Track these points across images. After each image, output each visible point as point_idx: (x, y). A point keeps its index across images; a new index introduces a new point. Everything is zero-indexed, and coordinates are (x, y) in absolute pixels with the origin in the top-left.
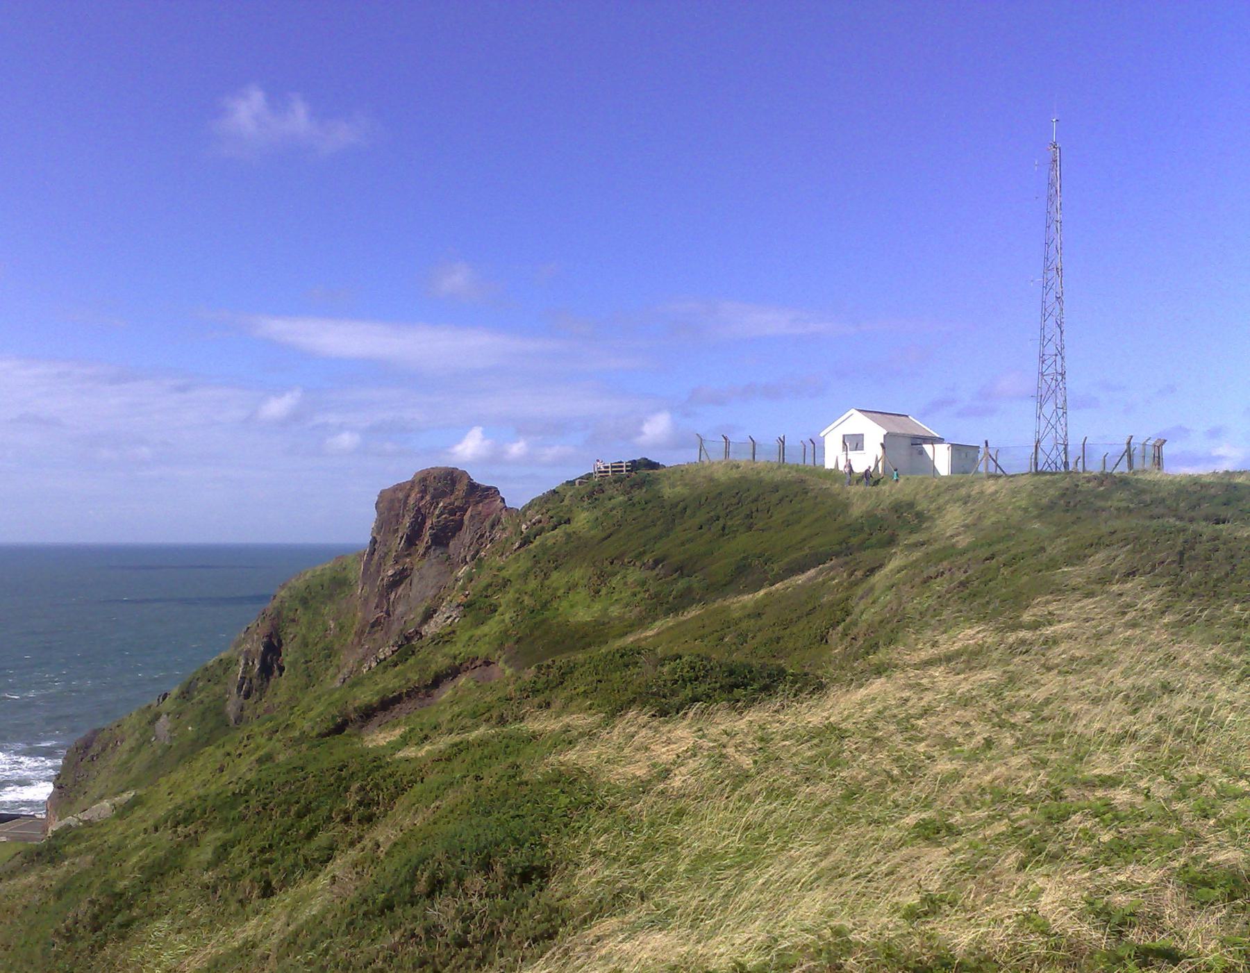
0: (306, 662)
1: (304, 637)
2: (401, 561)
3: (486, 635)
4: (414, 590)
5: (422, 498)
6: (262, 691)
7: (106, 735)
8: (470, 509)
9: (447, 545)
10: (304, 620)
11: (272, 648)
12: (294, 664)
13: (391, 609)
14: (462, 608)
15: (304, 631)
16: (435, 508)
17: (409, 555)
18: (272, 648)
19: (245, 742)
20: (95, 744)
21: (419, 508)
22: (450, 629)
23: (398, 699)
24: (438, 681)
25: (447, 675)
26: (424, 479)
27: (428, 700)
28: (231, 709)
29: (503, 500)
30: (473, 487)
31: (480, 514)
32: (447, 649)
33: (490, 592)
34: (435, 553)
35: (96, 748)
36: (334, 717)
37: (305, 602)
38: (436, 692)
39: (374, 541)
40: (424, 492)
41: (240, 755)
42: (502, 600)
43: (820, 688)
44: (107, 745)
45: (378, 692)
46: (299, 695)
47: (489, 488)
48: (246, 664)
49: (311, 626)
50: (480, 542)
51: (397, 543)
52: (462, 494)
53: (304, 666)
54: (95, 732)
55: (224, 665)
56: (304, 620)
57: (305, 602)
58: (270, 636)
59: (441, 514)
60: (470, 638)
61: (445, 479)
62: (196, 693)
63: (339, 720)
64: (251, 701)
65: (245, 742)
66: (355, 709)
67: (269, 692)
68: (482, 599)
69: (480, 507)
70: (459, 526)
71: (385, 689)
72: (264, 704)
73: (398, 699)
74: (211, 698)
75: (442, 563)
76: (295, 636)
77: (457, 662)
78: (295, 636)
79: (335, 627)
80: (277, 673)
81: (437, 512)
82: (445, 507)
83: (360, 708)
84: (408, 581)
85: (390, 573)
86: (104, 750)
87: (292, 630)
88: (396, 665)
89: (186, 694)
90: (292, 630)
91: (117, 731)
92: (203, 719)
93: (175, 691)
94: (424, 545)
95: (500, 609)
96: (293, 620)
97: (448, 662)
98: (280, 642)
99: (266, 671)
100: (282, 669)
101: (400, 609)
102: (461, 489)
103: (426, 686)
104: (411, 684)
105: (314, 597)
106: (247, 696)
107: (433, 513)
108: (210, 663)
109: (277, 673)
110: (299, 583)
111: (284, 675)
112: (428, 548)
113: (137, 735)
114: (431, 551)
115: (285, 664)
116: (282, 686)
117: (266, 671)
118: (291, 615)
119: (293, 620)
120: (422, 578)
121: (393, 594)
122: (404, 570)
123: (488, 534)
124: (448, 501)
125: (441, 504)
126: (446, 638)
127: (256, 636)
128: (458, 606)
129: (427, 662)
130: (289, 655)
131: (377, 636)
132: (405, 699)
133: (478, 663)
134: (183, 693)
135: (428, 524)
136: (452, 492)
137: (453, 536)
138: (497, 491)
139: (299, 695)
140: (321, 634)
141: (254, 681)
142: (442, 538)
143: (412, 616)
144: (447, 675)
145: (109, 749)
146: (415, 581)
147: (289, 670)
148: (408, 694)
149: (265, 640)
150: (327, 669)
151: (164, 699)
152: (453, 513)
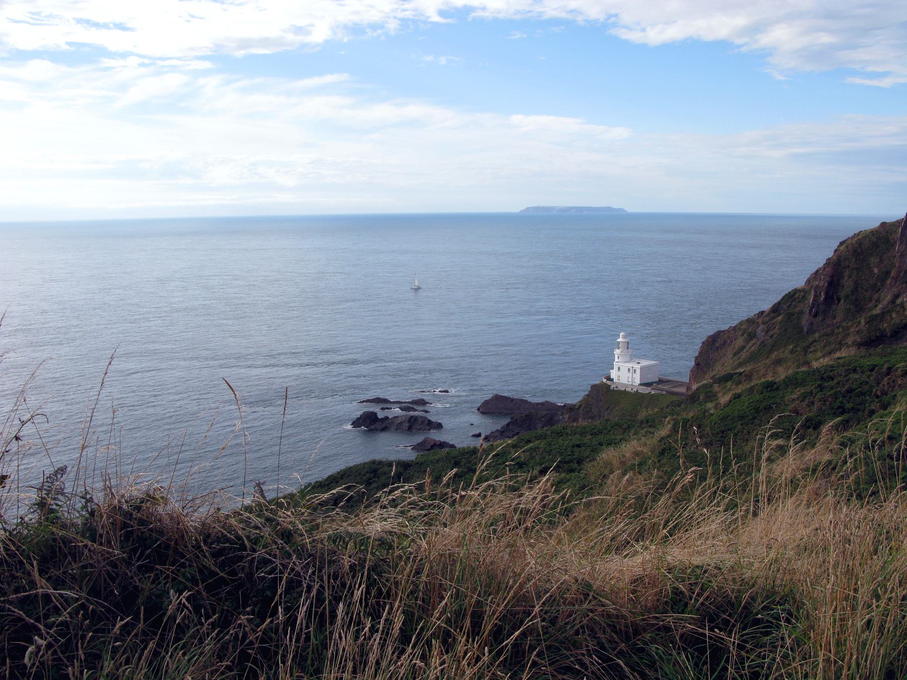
58: (832, 276)
64: (820, 318)
80: (836, 301)
100: (839, 300)
106: (816, 316)
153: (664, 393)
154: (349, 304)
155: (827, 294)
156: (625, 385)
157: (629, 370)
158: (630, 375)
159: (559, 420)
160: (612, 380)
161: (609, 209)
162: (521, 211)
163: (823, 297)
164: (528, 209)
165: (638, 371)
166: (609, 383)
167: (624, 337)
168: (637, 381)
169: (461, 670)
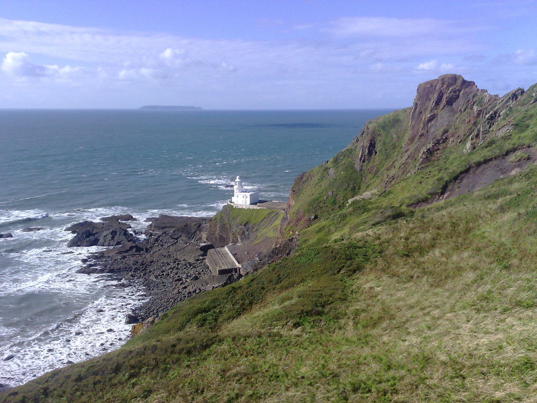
0: (386, 150)
1: (384, 141)
2: (433, 111)
3: (526, 136)
4: (438, 122)
5: (442, 86)
6: (369, 160)
7: (308, 174)
8: (463, 90)
9: (452, 105)
10: (383, 135)
11: (372, 145)
12: (381, 151)
13: (429, 130)
14: (513, 126)
15: (384, 138)
16: (448, 90)
17: (436, 109)
18: (372, 145)
19: (428, 174)
20: (304, 177)
21: (441, 91)
22: (509, 134)
23: (491, 160)
24: (508, 153)
25: (511, 151)
26: (443, 79)
27: (503, 160)
28: (357, 167)
29: (476, 86)
30: (464, 82)
31: (466, 92)
32: (509, 141)
33: (525, 120)
34: (447, 108)
35: (305, 179)
36: (466, 166)
37: (383, 128)
38: (506, 157)
39: (416, 104)
40: (443, 84)
41: (428, 178)
42: (531, 123)
43: (437, 180)
44: (308, 178)
45: (482, 157)
46: (383, 162)
47: (470, 82)
48: (363, 150)
49: (386, 136)
50: (468, 103)
51: (431, 104)
52: (459, 84)
53: (385, 152)
54: (304, 173)
55: (349, 151)
56: (383, 135)
57: (383, 128)
58: (371, 141)
59: (451, 92)
60: (519, 137)
61: (453, 79)
62: (340, 161)
63: (468, 167)
64: (365, 163)
65: (428, 174)
66: (474, 163)
67: (372, 160)
68: (522, 122)
69: (467, 89)
70: (458, 97)
71: (484, 156)
72: (370, 165)
73: (491, 160)
74: (348, 163)
75: (450, 112)
76: (380, 141)
77: (516, 146)
78: (380, 141)
79: (396, 137)
80: (374, 154)
81: (449, 92)
82: (452, 90)
83: (476, 162)
84: (436, 119)
85: (429, 116)
86: (307, 179)
87: (379, 138)
88: (487, 147)
89: (336, 161)
90: (379, 138)
91: (311, 173)
92: (347, 170)
93: (331, 160)
94: (443, 105)
95: (531, 126)
96: (379, 135)
97: (511, 146)
98: (375, 142)
99: (370, 153)
100: (376, 153)
101: (432, 130)
102: (459, 82)
103: (503, 155)
104: (496, 154)
105: (387, 126)
106: (364, 162)
107: (447, 93)
108: (343, 150)
109: (374, 154)
110: (381, 120)
111: (377, 154)
112: (445, 106)
113: (319, 175)
114: (446, 107)
115: (377, 151)
116: (377, 159)
117: (370, 153)
118: (378, 132)
119: (379, 135)
120: (442, 118)
121: (429, 124)
122: (434, 115)
123: (471, 100)
124: (454, 87)
125: (451, 89)
126: (508, 137)
127: (365, 141)
128: (512, 125)
129: (502, 146)
130: (378, 147)
131: (422, 140)
132: (493, 159)
133: (524, 147)
134: (334, 161)
135: (445, 97)
136: (455, 84)
137: (455, 101)
138: (474, 83)
139: (383, 162)
140: (391, 140)
141: (366, 157)
142: (450, 102)
143: (438, 132)
144: (511, 151)
145: (309, 179)
146: (439, 119)
147: (379, 153)
148: (495, 158)
149: (369, 142)
150: (394, 153)
151: (327, 163)
152: (455, 92)
153: (265, 208)
154: (148, 164)
155: (369, 149)
156: (241, 205)
157: (243, 196)
158: (244, 199)
159: (204, 227)
160: (234, 203)
161: (193, 107)
162: (140, 108)
163: (367, 152)
164: (145, 107)
165: (249, 197)
166: (232, 204)
167: (239, 179)
168: (248, 202)
169: (51, 237)
